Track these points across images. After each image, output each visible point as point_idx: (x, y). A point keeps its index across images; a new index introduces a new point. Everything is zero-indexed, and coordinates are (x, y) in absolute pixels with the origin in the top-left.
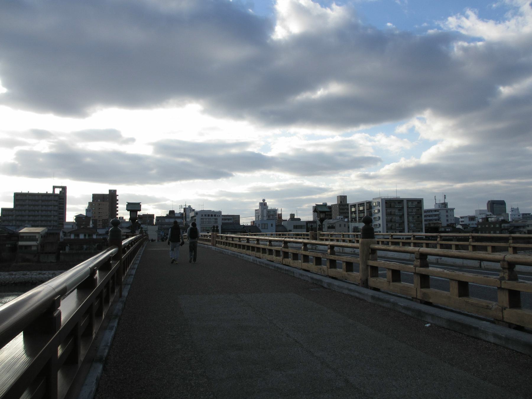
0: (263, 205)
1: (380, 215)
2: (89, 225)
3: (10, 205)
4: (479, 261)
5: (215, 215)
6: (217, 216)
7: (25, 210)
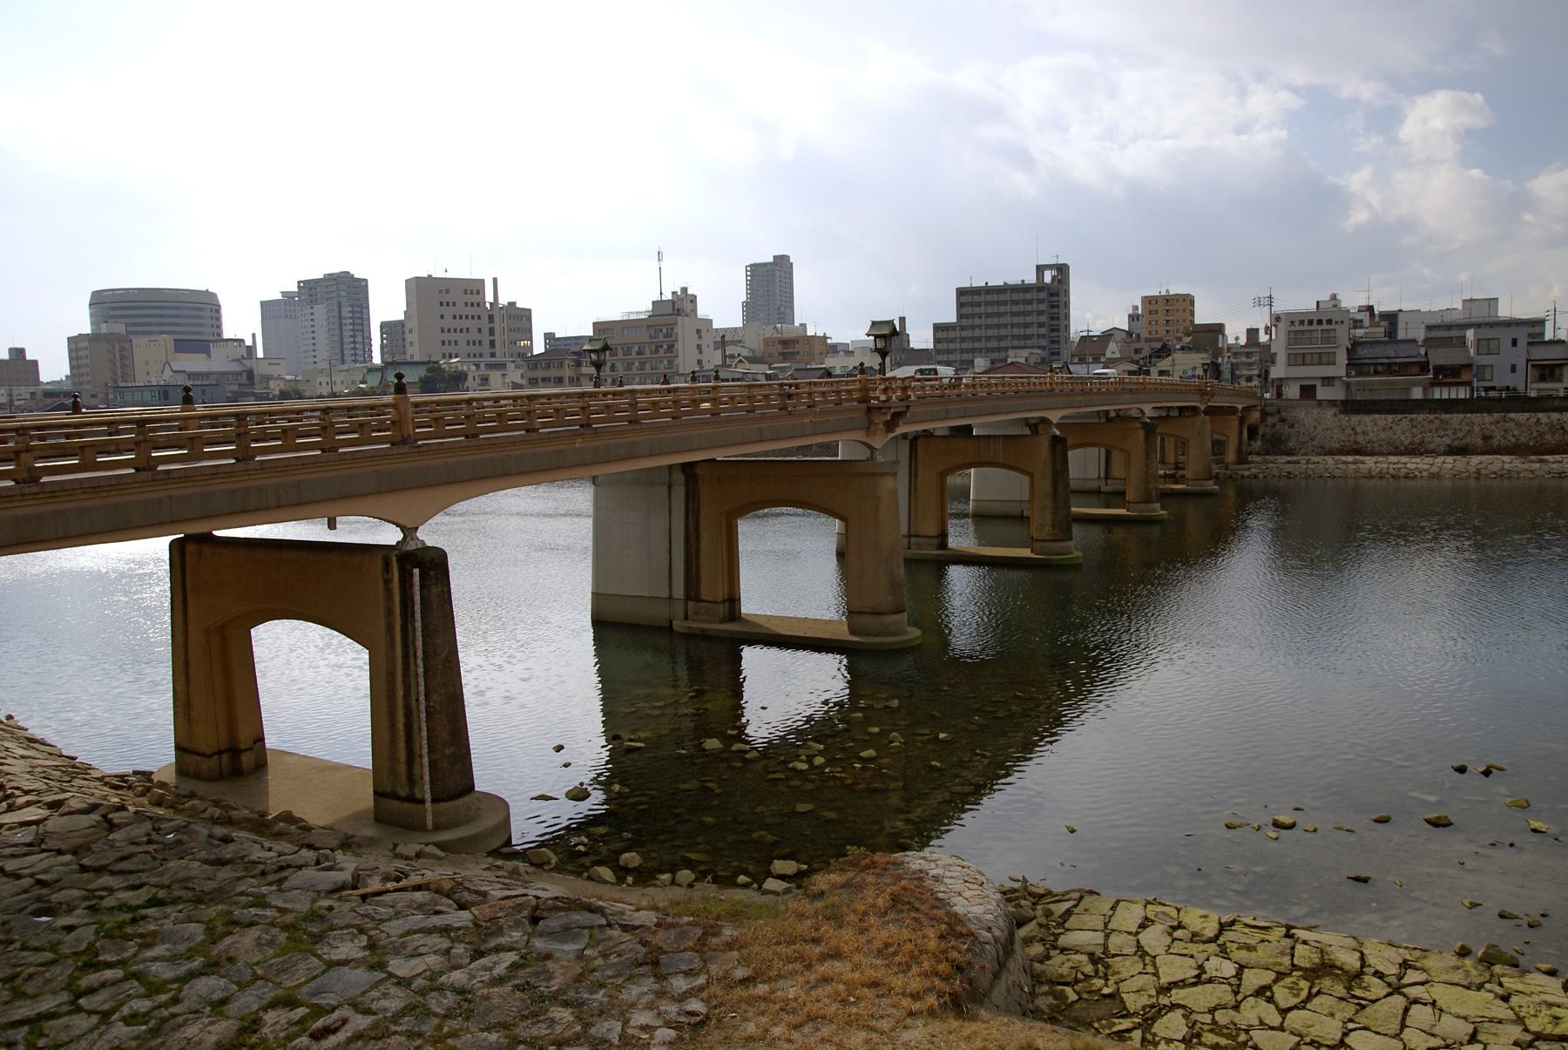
3: (950, 316)
5: (1329, 322)
6: (1336, 322)
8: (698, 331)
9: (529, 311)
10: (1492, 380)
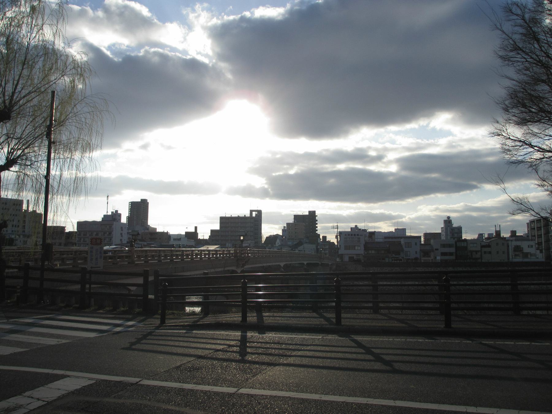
2: (275, 244)
3: (217, 227)
5: (358, 235)
8: (122, 228)
9: (220, 217)
10: (410, 256)
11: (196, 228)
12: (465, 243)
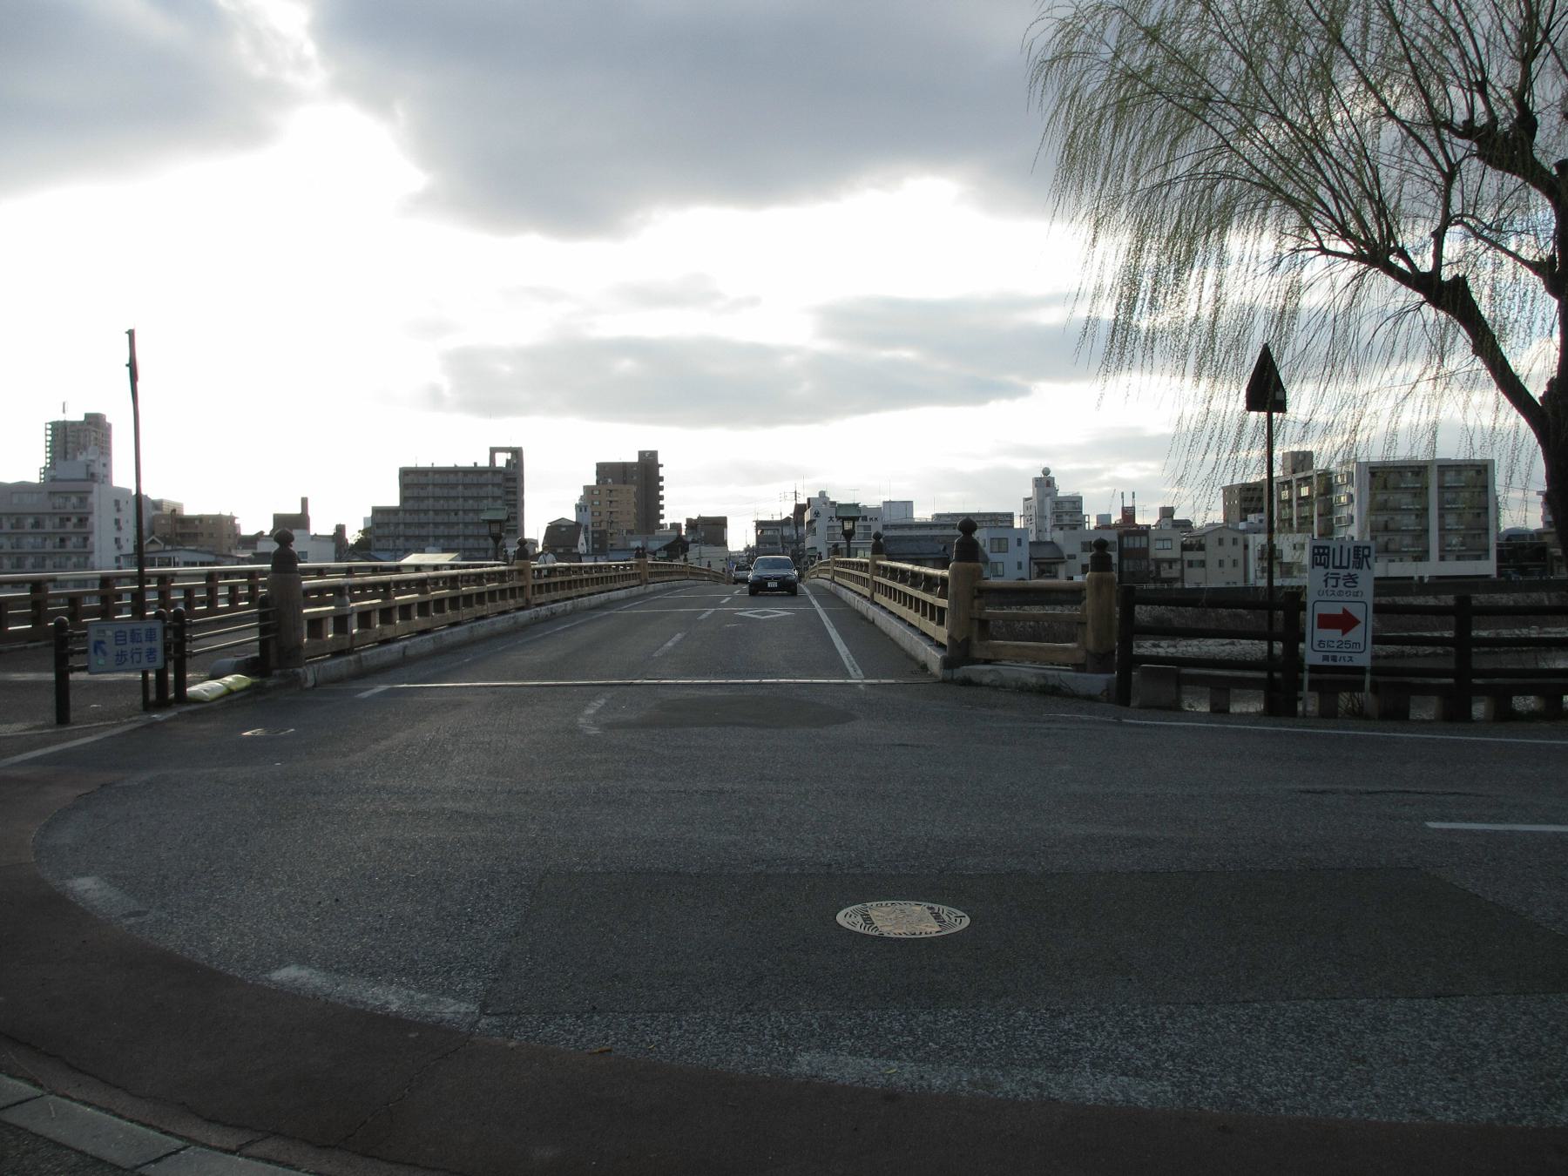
0: (1045, 483)
1: (1354, 510)
2: (577, 547)
3: (392, 498)
4: (1265, 612)
6: (871, 519)
7: (426, 511)
8: (117, 503)
11: (304, 502)
12: (1144, 539)
